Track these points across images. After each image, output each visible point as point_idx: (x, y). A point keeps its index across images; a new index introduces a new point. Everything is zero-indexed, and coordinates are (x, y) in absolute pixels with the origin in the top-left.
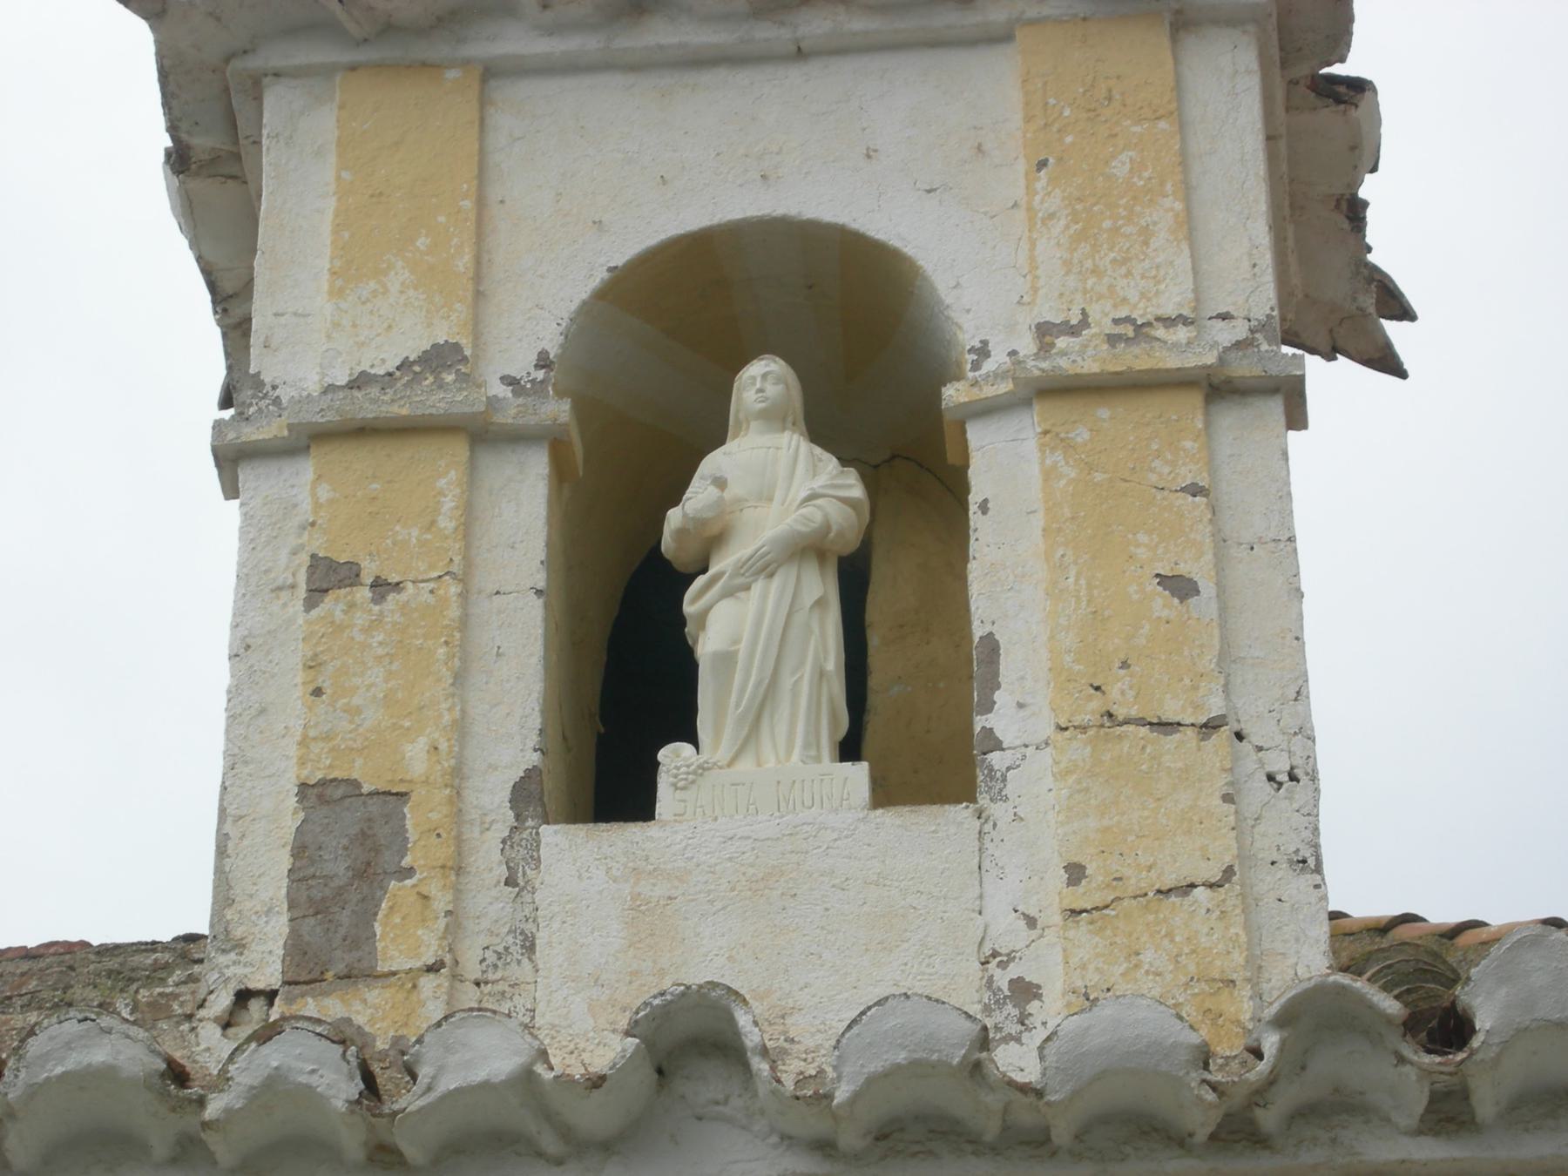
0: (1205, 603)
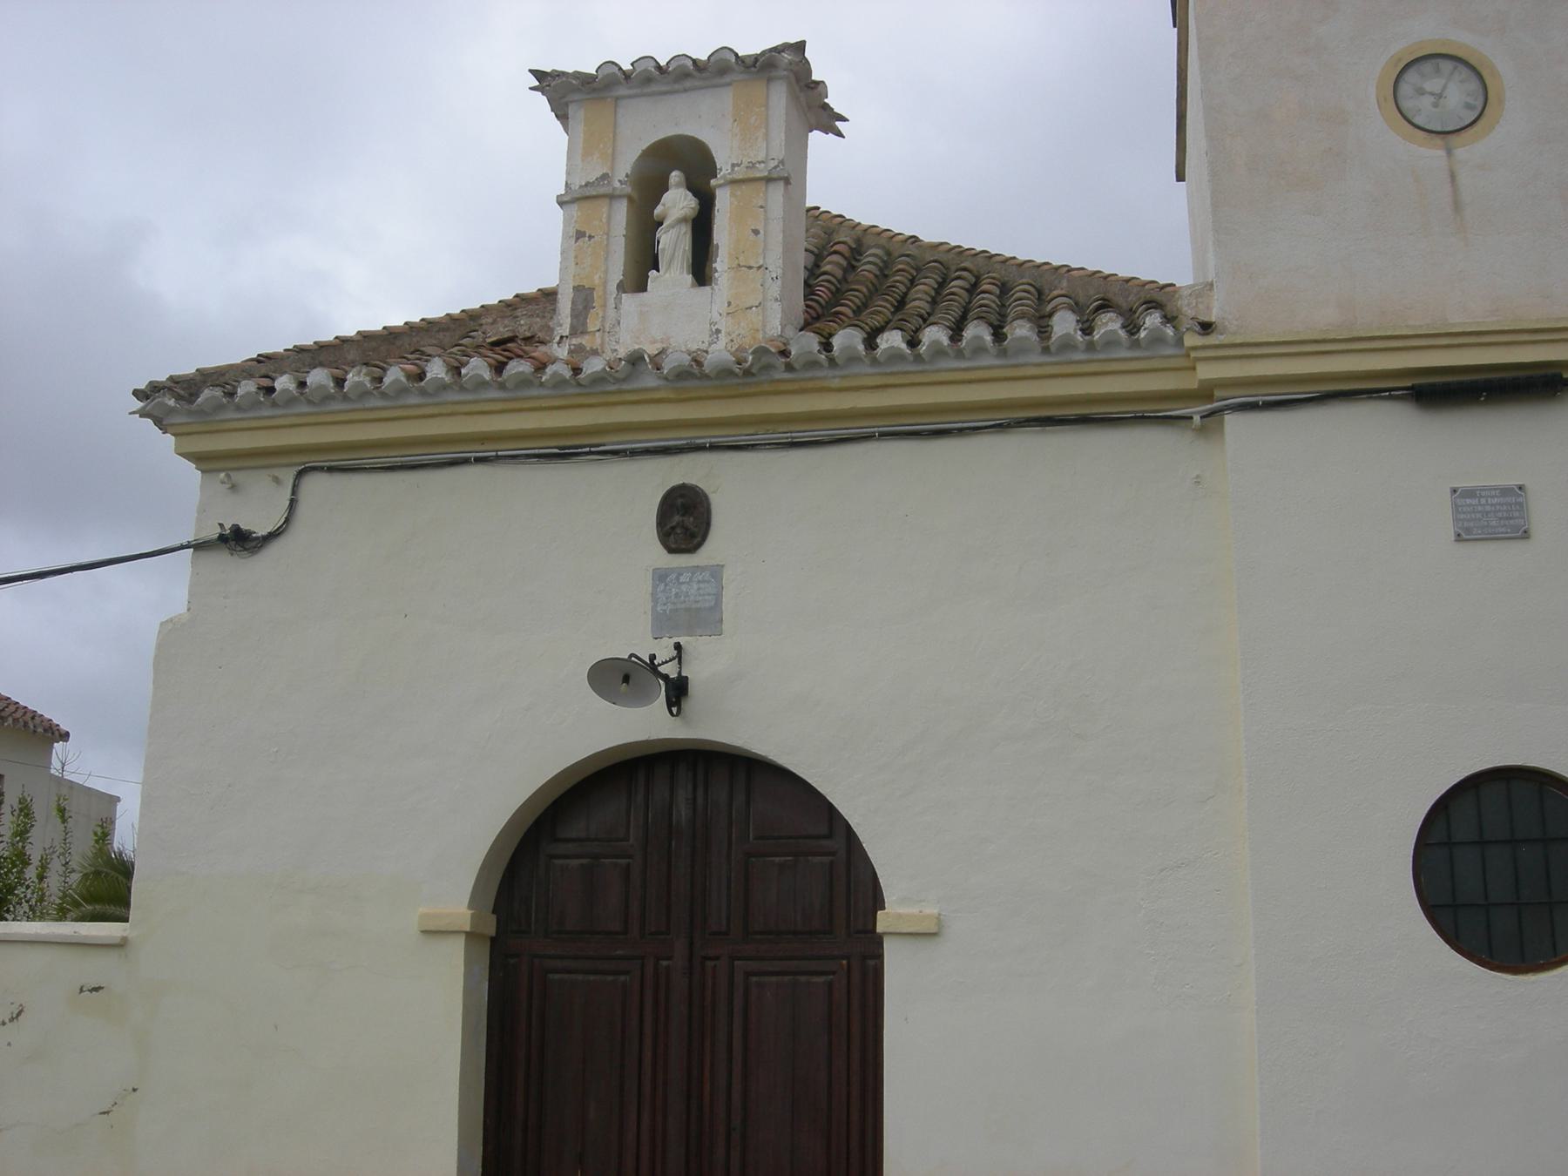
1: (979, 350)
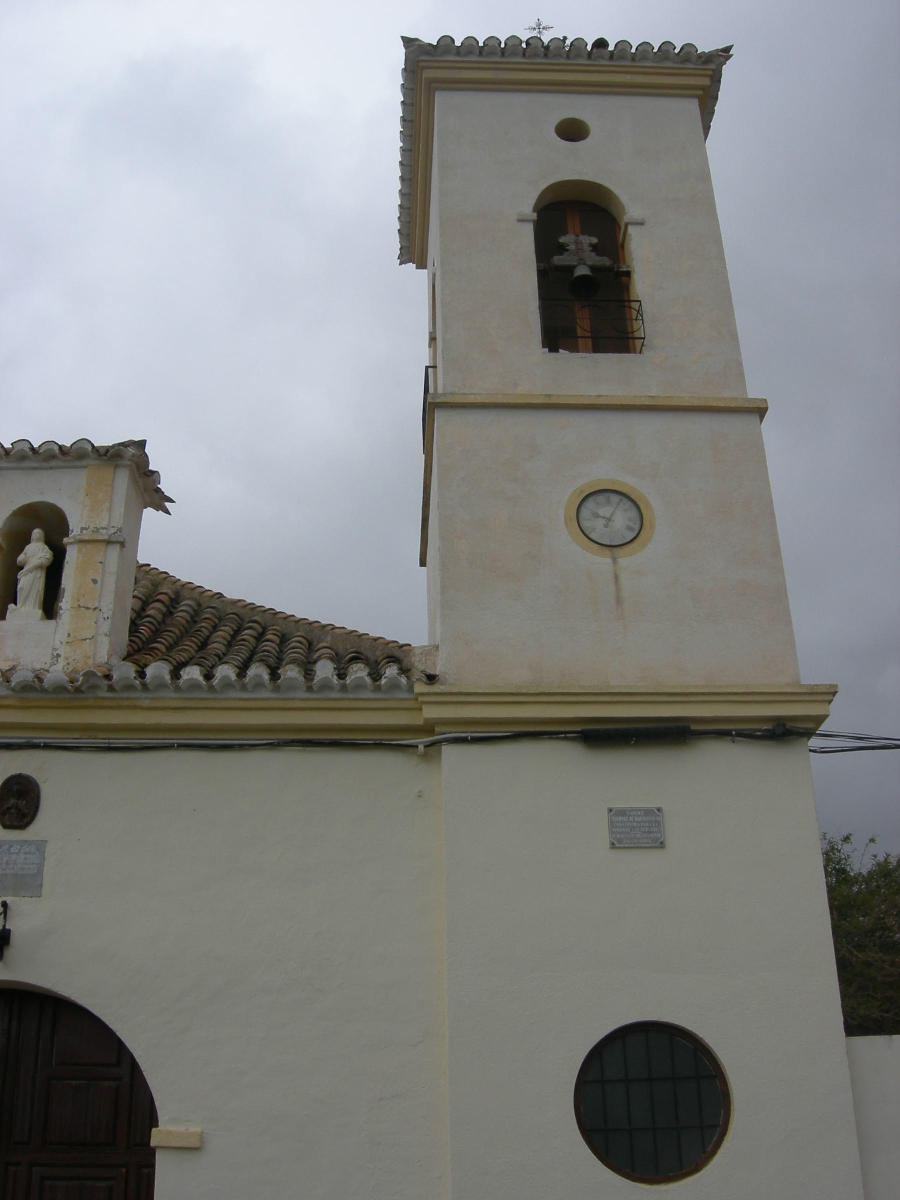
1: (259, 685)
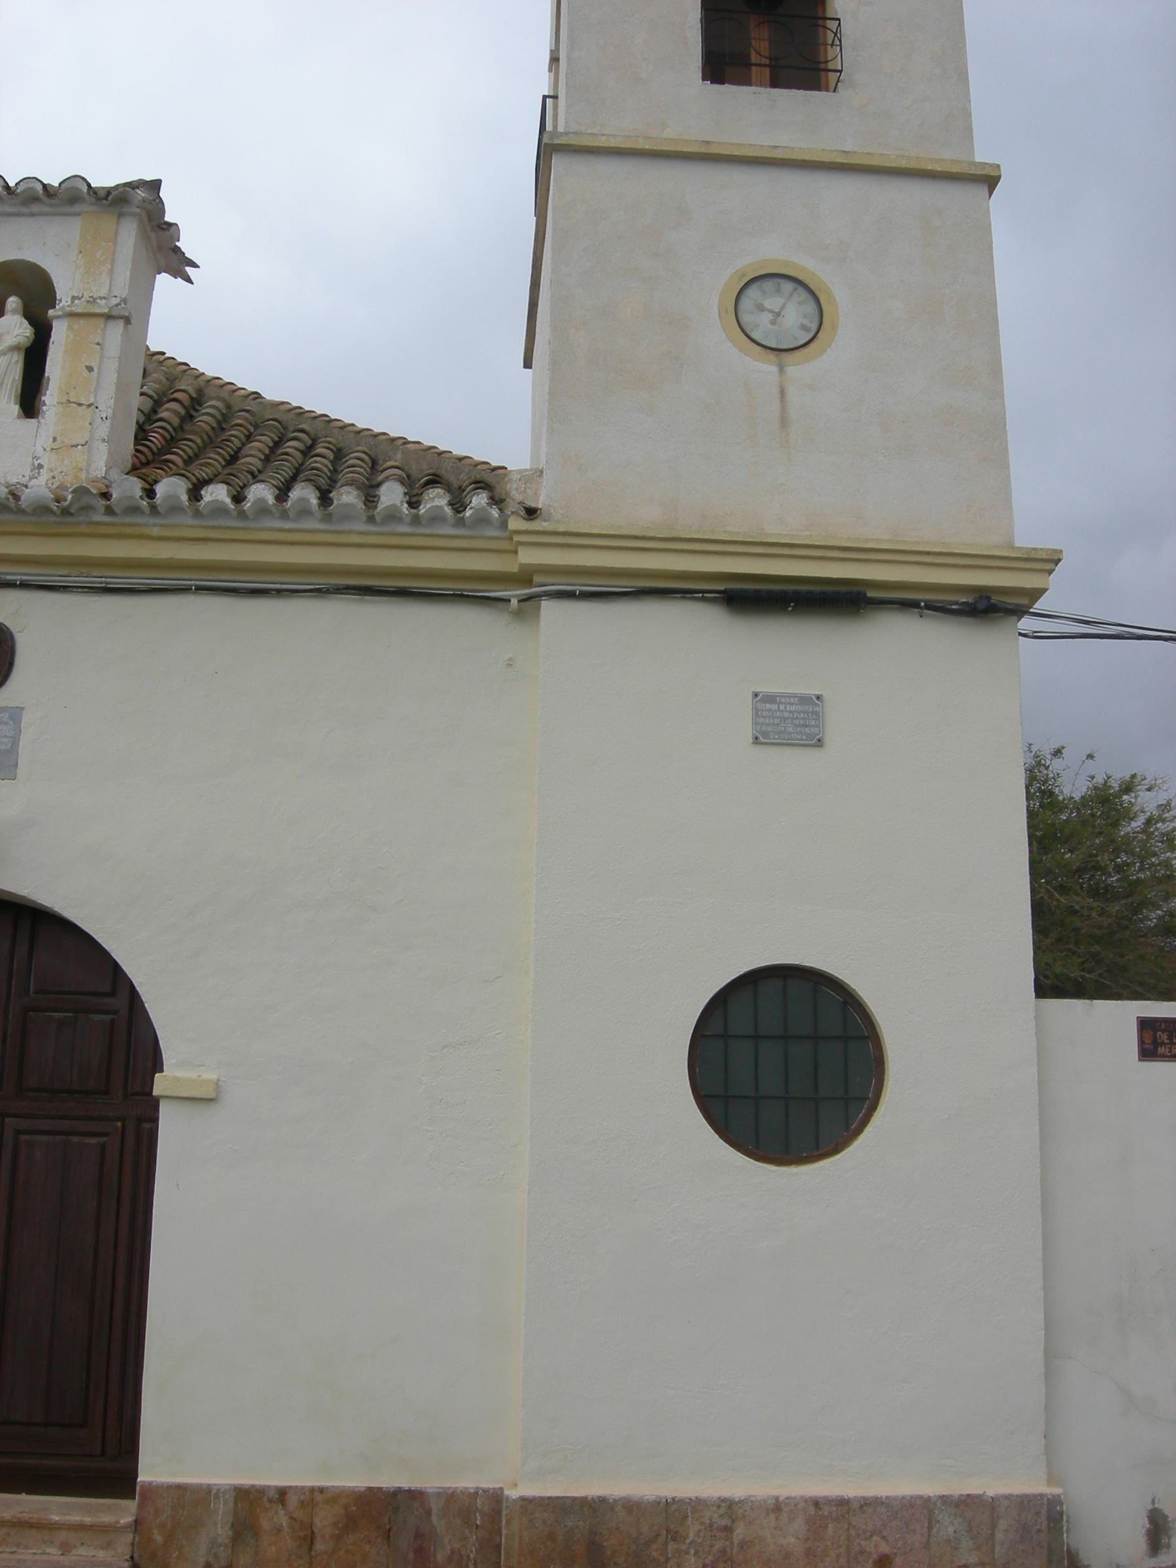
0: (95, 374)
1: (304, 512)
